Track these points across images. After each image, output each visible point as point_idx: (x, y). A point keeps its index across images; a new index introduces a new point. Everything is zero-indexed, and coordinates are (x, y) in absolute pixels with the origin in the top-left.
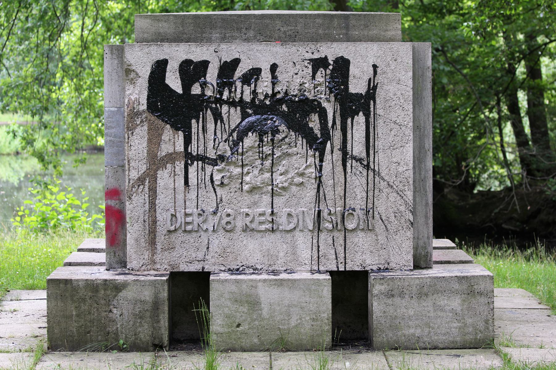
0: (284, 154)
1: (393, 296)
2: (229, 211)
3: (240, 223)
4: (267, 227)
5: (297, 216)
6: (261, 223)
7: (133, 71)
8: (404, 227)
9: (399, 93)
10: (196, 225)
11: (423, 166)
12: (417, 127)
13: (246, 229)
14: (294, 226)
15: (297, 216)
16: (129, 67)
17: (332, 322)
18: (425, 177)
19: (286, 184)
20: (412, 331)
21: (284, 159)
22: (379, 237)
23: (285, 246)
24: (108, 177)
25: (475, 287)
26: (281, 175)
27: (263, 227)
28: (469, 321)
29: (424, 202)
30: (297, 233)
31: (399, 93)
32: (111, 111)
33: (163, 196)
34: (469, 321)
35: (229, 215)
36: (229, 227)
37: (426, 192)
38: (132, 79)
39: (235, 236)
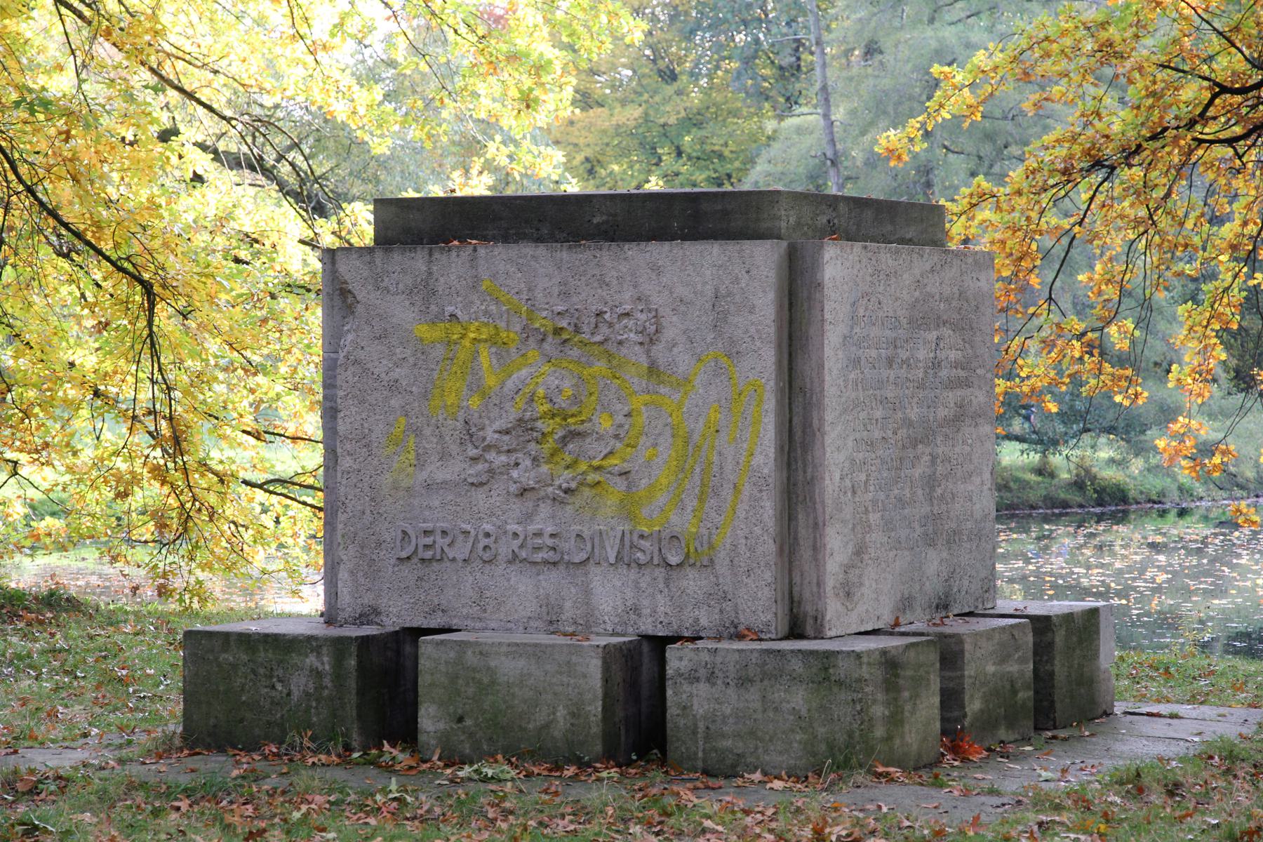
1: (698, 680)
2: (488, 527)
3: (504, 550)
4: (545, 556)
5: (592, 539)
6: (538, 549)
8: (762, 563)
9: (752, 330)
10: (439, 551)
11: (810, 458)
13: (514, 558)
14: (585, 556)
15: (592, 539)
17: (184, 692)
18: (812, 478)
19: (573, 485)
20: (728, 743)
23: (573, 590)
25: (831, 671)
26: (568, 467)
27: (539, 557)
28: (821, 731)
29: (811, 521)
30: (592, 568)
33: (391, 500)
34: (821, 731)
35: (487, 535)
36: (486, 556)
37: (815, 503)
39: (499, 570)
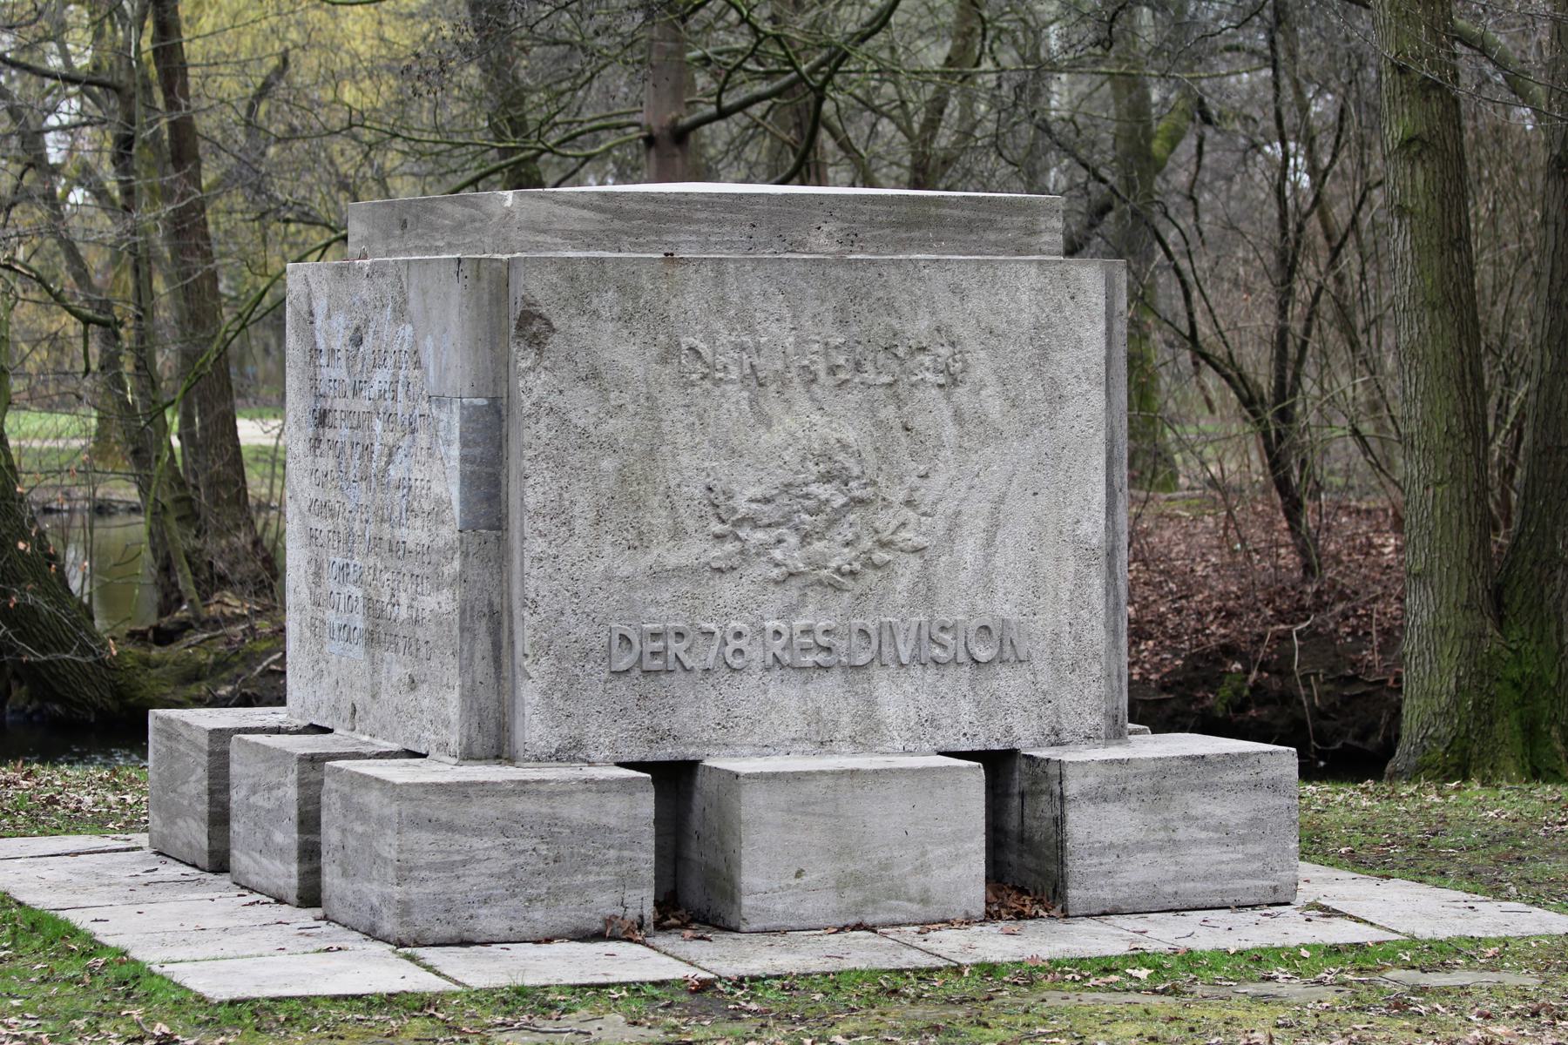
0: (852, 499)
6: (805, 650)
7: (540, 316)
10: (672, 658)
12: (1111, 443)
16: (532, 309)
21: (850, 511)
22: (1039, 678)
23: (852, 700)
24: (467, 555)
30: (876, 671)
31: (1079, 369)
32: (475, 407)
35: (739, 635)
38: (535, 336)
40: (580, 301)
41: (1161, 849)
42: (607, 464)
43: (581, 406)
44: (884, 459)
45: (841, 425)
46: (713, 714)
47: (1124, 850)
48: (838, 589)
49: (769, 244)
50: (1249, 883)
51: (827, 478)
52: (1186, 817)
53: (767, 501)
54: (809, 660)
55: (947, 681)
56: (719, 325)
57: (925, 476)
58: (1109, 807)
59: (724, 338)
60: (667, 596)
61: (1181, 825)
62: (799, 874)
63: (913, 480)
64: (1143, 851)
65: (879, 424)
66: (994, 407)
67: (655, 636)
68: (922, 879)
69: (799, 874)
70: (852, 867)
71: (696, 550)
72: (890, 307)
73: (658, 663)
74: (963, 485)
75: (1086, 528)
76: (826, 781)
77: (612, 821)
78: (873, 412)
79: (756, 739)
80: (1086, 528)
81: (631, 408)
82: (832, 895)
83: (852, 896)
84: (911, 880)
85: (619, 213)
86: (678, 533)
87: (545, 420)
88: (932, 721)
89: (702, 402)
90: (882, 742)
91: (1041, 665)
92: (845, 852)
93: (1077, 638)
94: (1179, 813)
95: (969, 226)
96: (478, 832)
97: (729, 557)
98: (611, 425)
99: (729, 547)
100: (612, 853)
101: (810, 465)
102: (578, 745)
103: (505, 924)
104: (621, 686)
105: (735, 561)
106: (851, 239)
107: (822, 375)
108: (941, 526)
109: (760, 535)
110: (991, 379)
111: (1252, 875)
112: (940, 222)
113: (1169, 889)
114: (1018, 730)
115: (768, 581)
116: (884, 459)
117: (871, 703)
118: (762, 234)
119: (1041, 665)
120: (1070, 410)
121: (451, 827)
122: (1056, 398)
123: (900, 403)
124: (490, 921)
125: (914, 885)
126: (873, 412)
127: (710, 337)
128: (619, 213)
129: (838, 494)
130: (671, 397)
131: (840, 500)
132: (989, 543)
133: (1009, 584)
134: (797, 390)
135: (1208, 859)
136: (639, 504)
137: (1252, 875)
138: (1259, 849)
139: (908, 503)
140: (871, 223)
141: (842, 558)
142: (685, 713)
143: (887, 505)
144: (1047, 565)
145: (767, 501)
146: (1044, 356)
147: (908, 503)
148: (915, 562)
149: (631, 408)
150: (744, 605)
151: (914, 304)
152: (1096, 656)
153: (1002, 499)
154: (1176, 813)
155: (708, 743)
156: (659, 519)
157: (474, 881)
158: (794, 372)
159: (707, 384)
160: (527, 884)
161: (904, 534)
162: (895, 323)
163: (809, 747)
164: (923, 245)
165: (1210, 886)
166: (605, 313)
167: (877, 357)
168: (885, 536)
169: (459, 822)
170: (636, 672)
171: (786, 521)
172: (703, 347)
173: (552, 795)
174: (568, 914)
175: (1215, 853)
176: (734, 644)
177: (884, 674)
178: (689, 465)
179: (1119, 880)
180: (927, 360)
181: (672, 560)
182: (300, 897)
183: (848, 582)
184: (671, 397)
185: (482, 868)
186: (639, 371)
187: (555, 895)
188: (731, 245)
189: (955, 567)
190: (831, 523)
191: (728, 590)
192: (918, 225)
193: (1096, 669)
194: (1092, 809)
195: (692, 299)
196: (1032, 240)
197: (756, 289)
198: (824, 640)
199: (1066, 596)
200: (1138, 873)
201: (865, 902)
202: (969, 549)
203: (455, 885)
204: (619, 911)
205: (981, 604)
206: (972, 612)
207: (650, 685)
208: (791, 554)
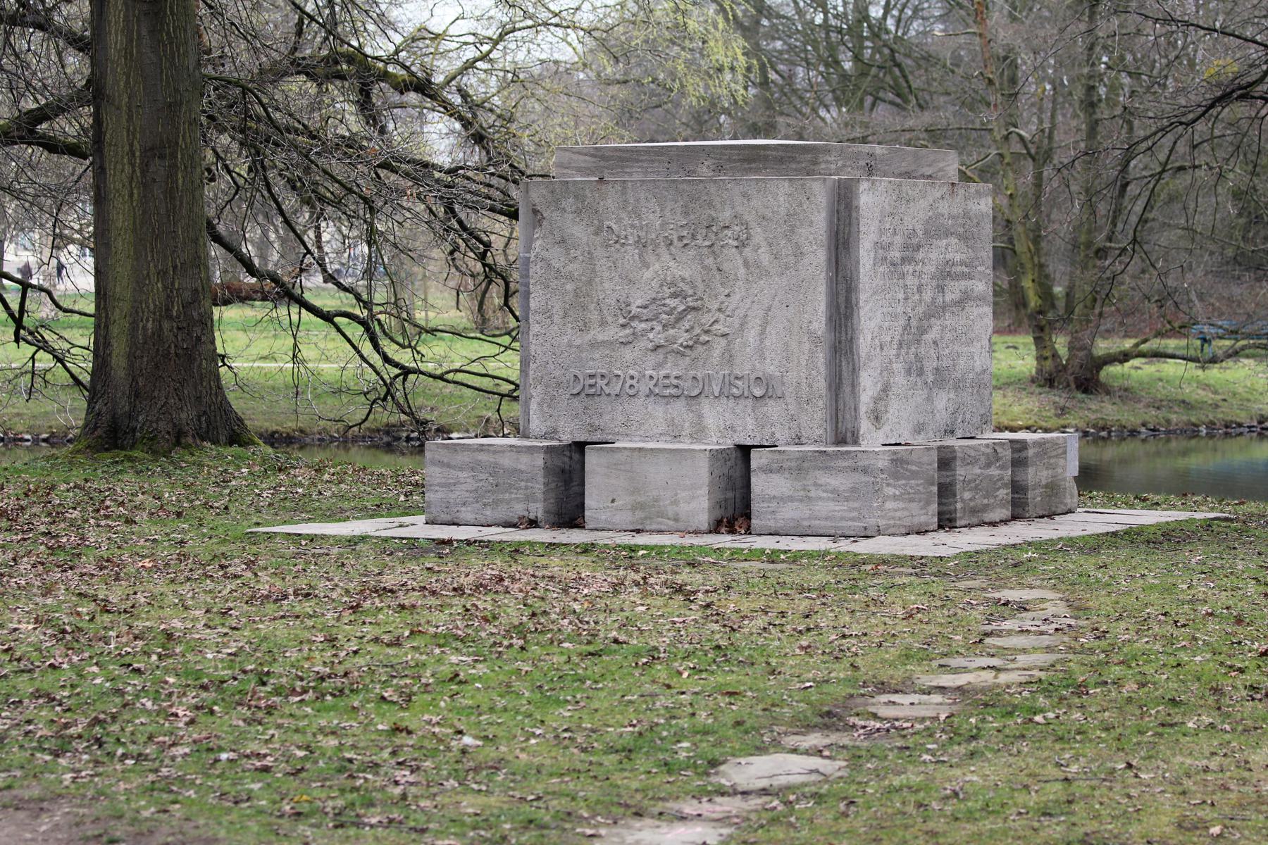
6: (666, 387)
30: (702, 398)
31: (811, 238)
35: (632, 378)
40: (556, 204)
41: (801, 501)
42: (569, 287)
43: (557, 256)
44: (708, 286)
45: (682, 268)
46: (621, 419)
47: (782, 500)
48: (683, 355)
49: (677, 173)
50: (850, 523)
51: (674, 295)
52: (815, 484)
53: (645, 307)
54: (667, 392)
55: (740, 406)
56: (624, 215)
57: (728, 296)
58: (773, 476)
59: (626, 221)
60: (598, 356)
61: (812, 488)
62: (613, 501)
63: (722, 298)
64: (792, 501)
65: (705, 267)
66: (765, 257)
67: (591, 376)
68: (675, 508)
69: (613, 501)
70: (639, 499)
71: (613, 332)
72: (710, 205)
73: (593, 390)
74: (749, 301)
75: (815, 325)
76: (627, 453)
77: (523, 467)
78: (702, 260)
79: (642, 433)
80: (815, 325)
81: (581, 258)
82: (630, 513)
83: (640, 514)
84: (669, 508)
85: (603, 158)
86: (603, 323)
87: (540, 264)
88: (732, 427)
89: (616, 256)
90: (706, 438)
91: (790, 400)
92: (636, 491)
93: (810, 386)
94: (810, 482)
95: (781, 160)
96: (461, 469)
97: (627, 336)
98: (571, 267)
99: (628, 331)
100: (523, 484)
101: (665, 289)
102: (555, 431)
103: (474, 516)
104: (576, 401)
105: (630, 339)
106: (719, 169)
107: (675, 241)
108: (737, 322)
109: (643, 325)
110: (763, 243)
111: (852, 519)
112: (766, 158)
113: (806, 523)
114: (778, 435)
115: (647, 349)
116: (708, 286)
117: (700, 416)
118: (674, 167)
119: (790, 400)
120: (806, 261)
121: (449, 466)
122: (799, 254)
123: (715, 256)
124: (466, 514)
125: (671, 511)
126: (702, 260)
127: (619, 220)
128: (603, 158)
129: (684, 305)
130: (600, 252)
131: (683, 307)
132: (762, 333)
133: (773, 355)
134: (662, 249)
135: (826, 507)
136: (584, 308)
137: (852, 519)
138: (856, 505)
139: (720, 310)
140: (730, 160)
141: (683, 338)
142: (607, 417)
143: (709, 311)
144: (794, 346)
145: (645, 307)
146: (792, 231)
147: (720, 310)
148: (723, 342)
149: (581, 258)
150: (635, 362)
151: (723, 203)
152: (820, 396)
153: (769, 309)
154: (810, 482)
155: (618, 434)
156: (594, 316)
157: (459, 494)
158: (661, 239)
159: (618, 246)
160: (483, 497)
161: (716, 326)
162: (713, 213)
163: (669, 438)
164: (757, 171)
165: (829, 523)
166: (568, 210)
167: (705, 232)
168: (706, 327)
169: (453, 463)
170: (583, 395)
171: (656, 318)
172: (614, 226)
173: (495, 452)
174: (502, 513)
175: (832, 506)
176: (630, 382)
177: (707, 401)
178: (609, 289)
179: (778, 516)
180: (729, 233)
181: (600, 338)
182: (552, 518)
183: (688, 352)
184: (600, 252)
185: (463, 487)
186: (585, 239)
187: (497, 503)
188: (658, 173)
189: (745, 345)
190: (678, 320)
191: (628, 354)
192: (754, 161)
193: (820, 403)
194: (764, 476)
195: (611, 200)
196: (816, 168)
197: (642, 196)
198: (675, 382)
199: (804, 363)
200: (789, 513)
201: (646, 518)
202: (752, 336)
203: (450, 495)
204: (526, 514)
205: (758, 366)
206: (754, 369)
207: (590, 402)
208: (657, 336)
